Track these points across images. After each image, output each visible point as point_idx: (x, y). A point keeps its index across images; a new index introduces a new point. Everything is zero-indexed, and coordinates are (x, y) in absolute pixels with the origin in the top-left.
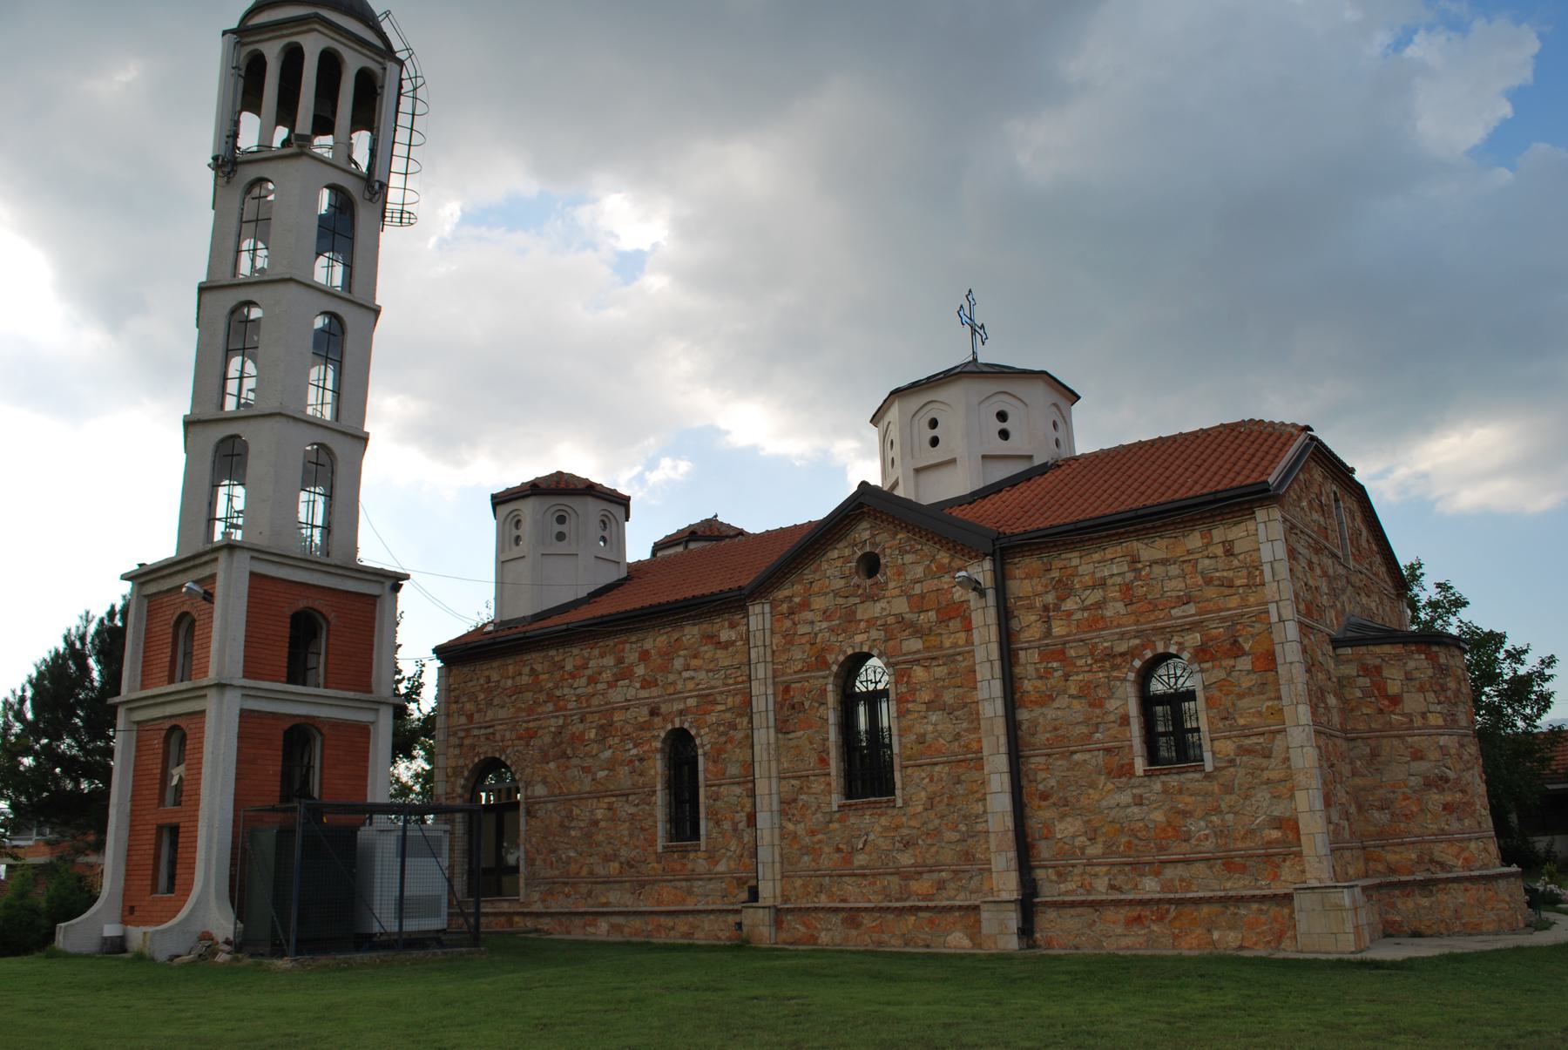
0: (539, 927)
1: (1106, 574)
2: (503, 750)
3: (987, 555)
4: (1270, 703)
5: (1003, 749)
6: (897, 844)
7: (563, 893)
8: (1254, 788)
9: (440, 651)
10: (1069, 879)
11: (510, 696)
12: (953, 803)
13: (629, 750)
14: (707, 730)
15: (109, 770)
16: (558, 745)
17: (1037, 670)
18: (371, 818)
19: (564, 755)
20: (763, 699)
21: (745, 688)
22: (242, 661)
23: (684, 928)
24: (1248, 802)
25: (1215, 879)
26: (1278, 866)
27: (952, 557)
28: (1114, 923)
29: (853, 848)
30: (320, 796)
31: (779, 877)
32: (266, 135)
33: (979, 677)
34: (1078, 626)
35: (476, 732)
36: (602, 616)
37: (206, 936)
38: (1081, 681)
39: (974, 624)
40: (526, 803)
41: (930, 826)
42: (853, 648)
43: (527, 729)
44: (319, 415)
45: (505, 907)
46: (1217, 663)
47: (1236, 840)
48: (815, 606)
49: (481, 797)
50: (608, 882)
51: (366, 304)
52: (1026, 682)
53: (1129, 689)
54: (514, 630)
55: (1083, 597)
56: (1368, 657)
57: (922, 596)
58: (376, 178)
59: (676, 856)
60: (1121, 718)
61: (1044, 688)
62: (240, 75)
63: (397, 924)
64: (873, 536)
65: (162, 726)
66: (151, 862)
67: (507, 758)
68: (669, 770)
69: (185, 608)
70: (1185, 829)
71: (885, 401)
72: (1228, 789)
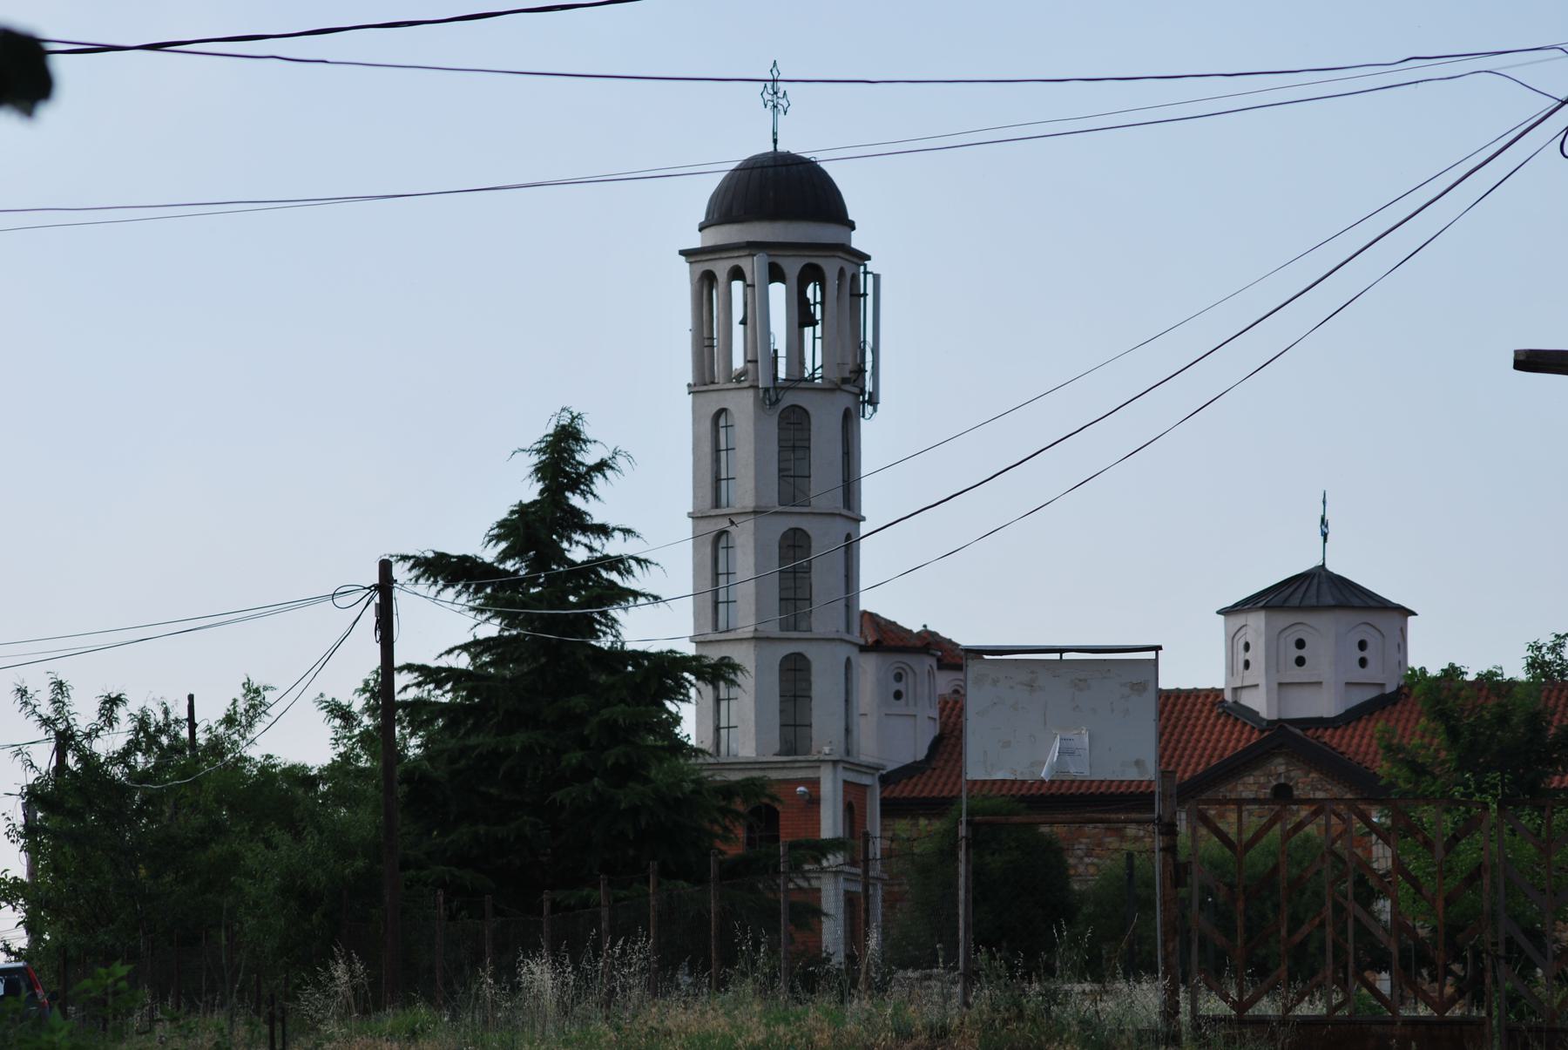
64: (1288, 771)
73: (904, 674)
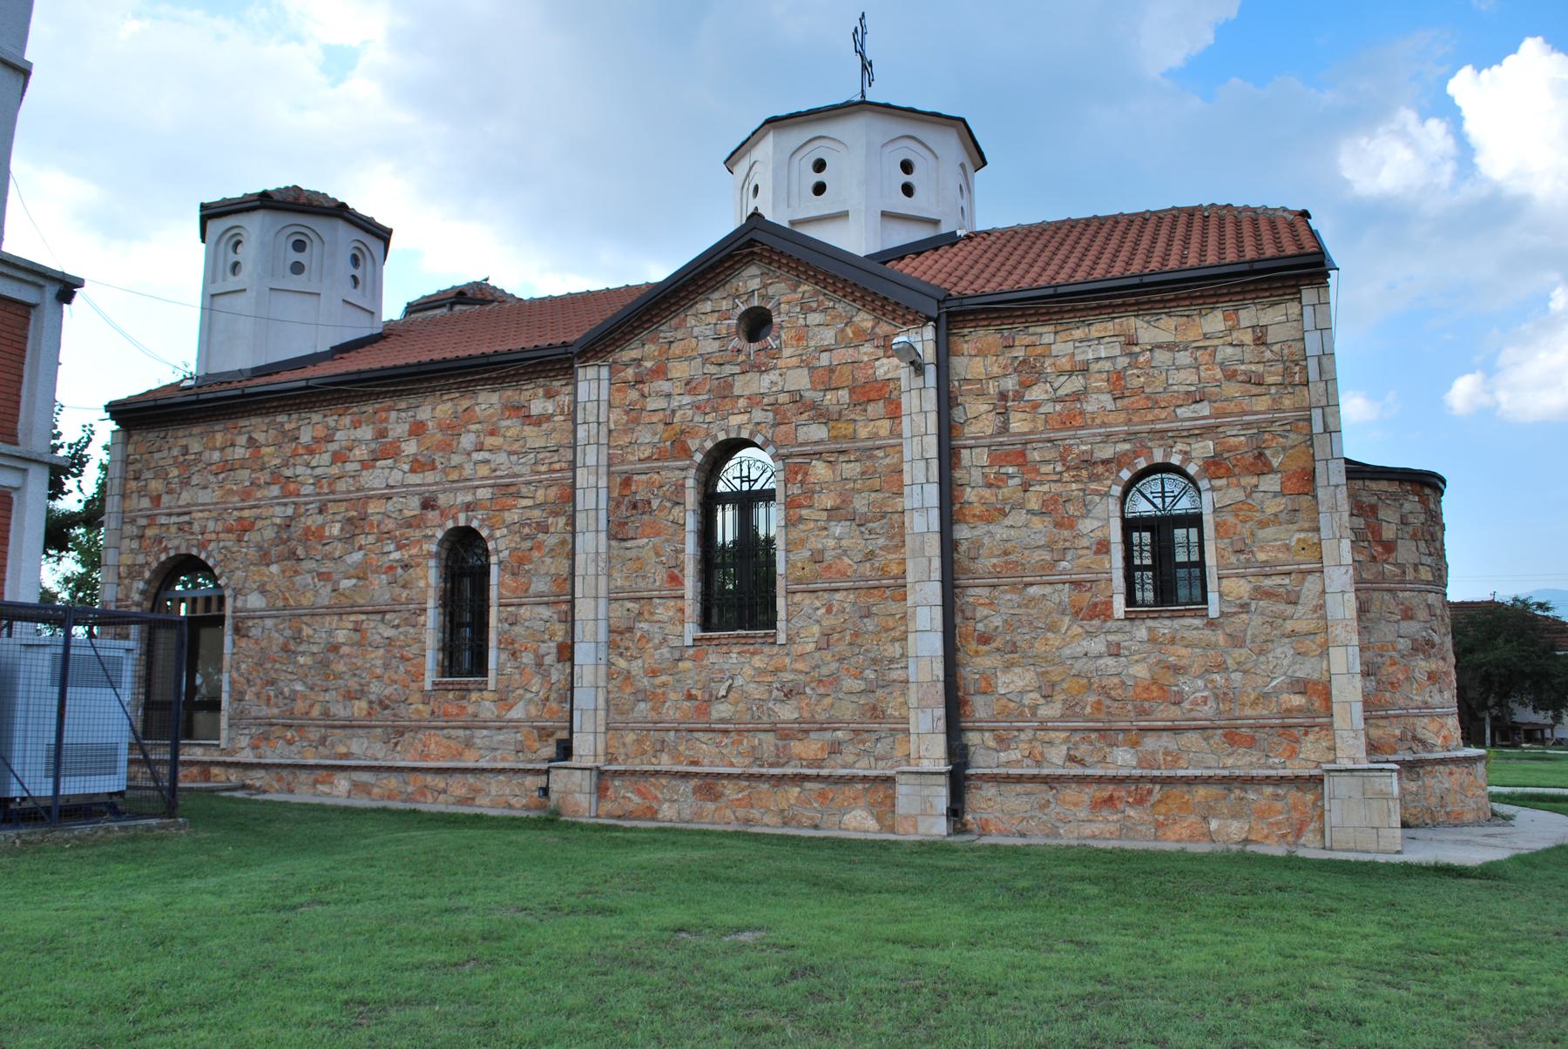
1: (1090, 356)
2: (203, 546)
3: (929, 319)
4: (1302, 535)
5: (937, 575)
6: (775, 693)
7: (284, 738)
8: (1272, 641)
10: (1013, 745)
11: (217, 474)
12: (859, 641)
14: (505, 531)
16: (285, 542)
17: (985, 475)
19: (293, 555)
20: (592, 494)
21: (564, 478)
23: (462, 792)
24: (1262, 659)
25: (1212, 752)
26: (1297, 741)
27: (877, 320)
28: (1076, 805)
29: (711, 695)
31: (602, 729)
33: (907, 479)
34: (1046, 422)
35: (163, 520)
38: (1045, 493)
39: (905, 408)
40: (234, 618)
41: (825, 671)
42: (727, 433)
46: (1234, 480)
47: (1244, 705)
48: (674, 374)
50: (349, 726)
52: (969, 490)
53: (1111, 508)
54: (225, 386)
55: (1056, 385)
56: (1364, 493)
57: (831, 370)
59: (451, 695)
60: (1098, 543)
61: (993, 499)
64: (765, 286)
68: (445, 582)
70: (1176, 689)
71: (754, 133)
72: (1237, 641)
73: (360, 257)
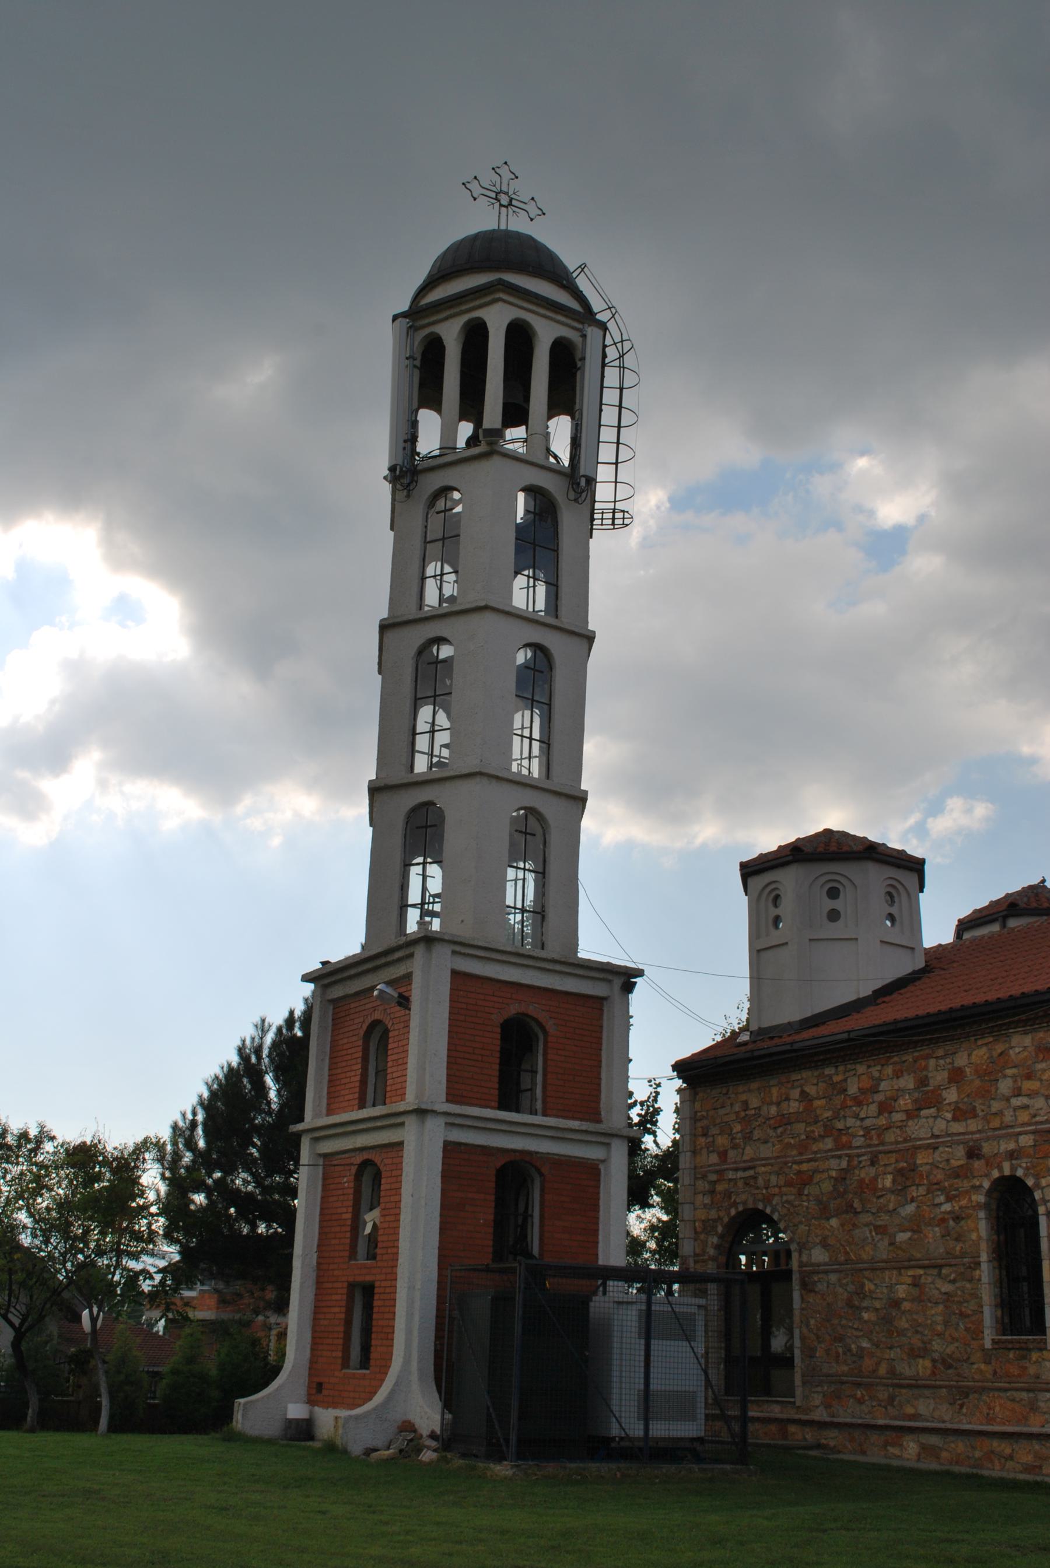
0: (823, 1441)
2: (767, 1200)
7: (854, 1396)
9: (682, 1068)
11: (775, 1128)
13: (941, 1204)
15: (292, 1212)
18: (604, 1285)
19: (850, 1208)
22: (444, 1081)
23: (1028, 1459)
30: (541, 1254)
32: (448, 433)
35: (731, 1175)
36: (896, 1022)
37: (407, 1427)
40: (800, 1272)
43: (799, 1172)
44: (525, 772)
45: (776, 1411)
49: (740, 1260)
50: (916, 1385)
51: (576, 630)
54: (776, 1041)
58: (582, 473)
59: (1011, 1355)
62: (415, 366)
63: (642, 1427)
65: (352, 1160)
66: (341, 1329)
67: (773, 1212)
68: (998, 1236)
69: (377, 1016)
73: (895, 894)
